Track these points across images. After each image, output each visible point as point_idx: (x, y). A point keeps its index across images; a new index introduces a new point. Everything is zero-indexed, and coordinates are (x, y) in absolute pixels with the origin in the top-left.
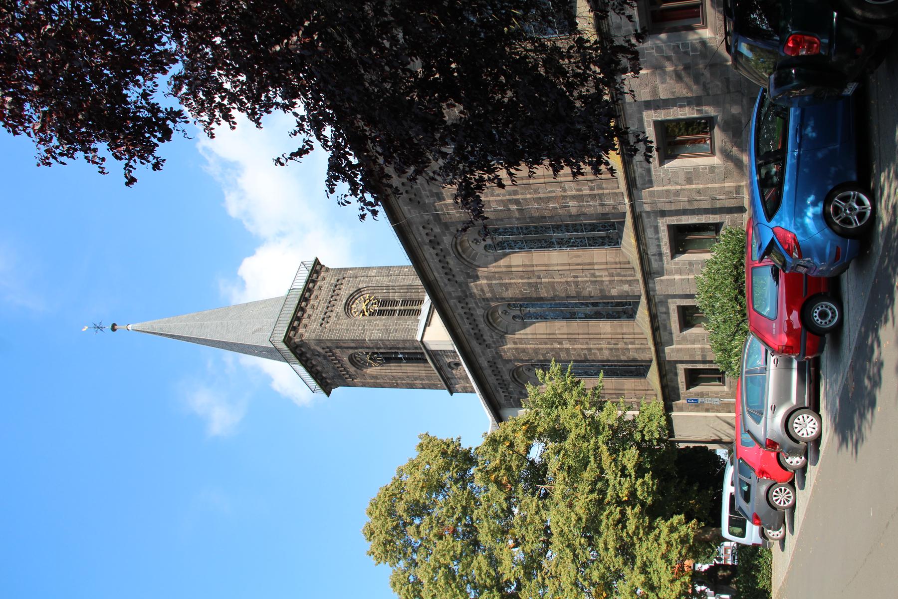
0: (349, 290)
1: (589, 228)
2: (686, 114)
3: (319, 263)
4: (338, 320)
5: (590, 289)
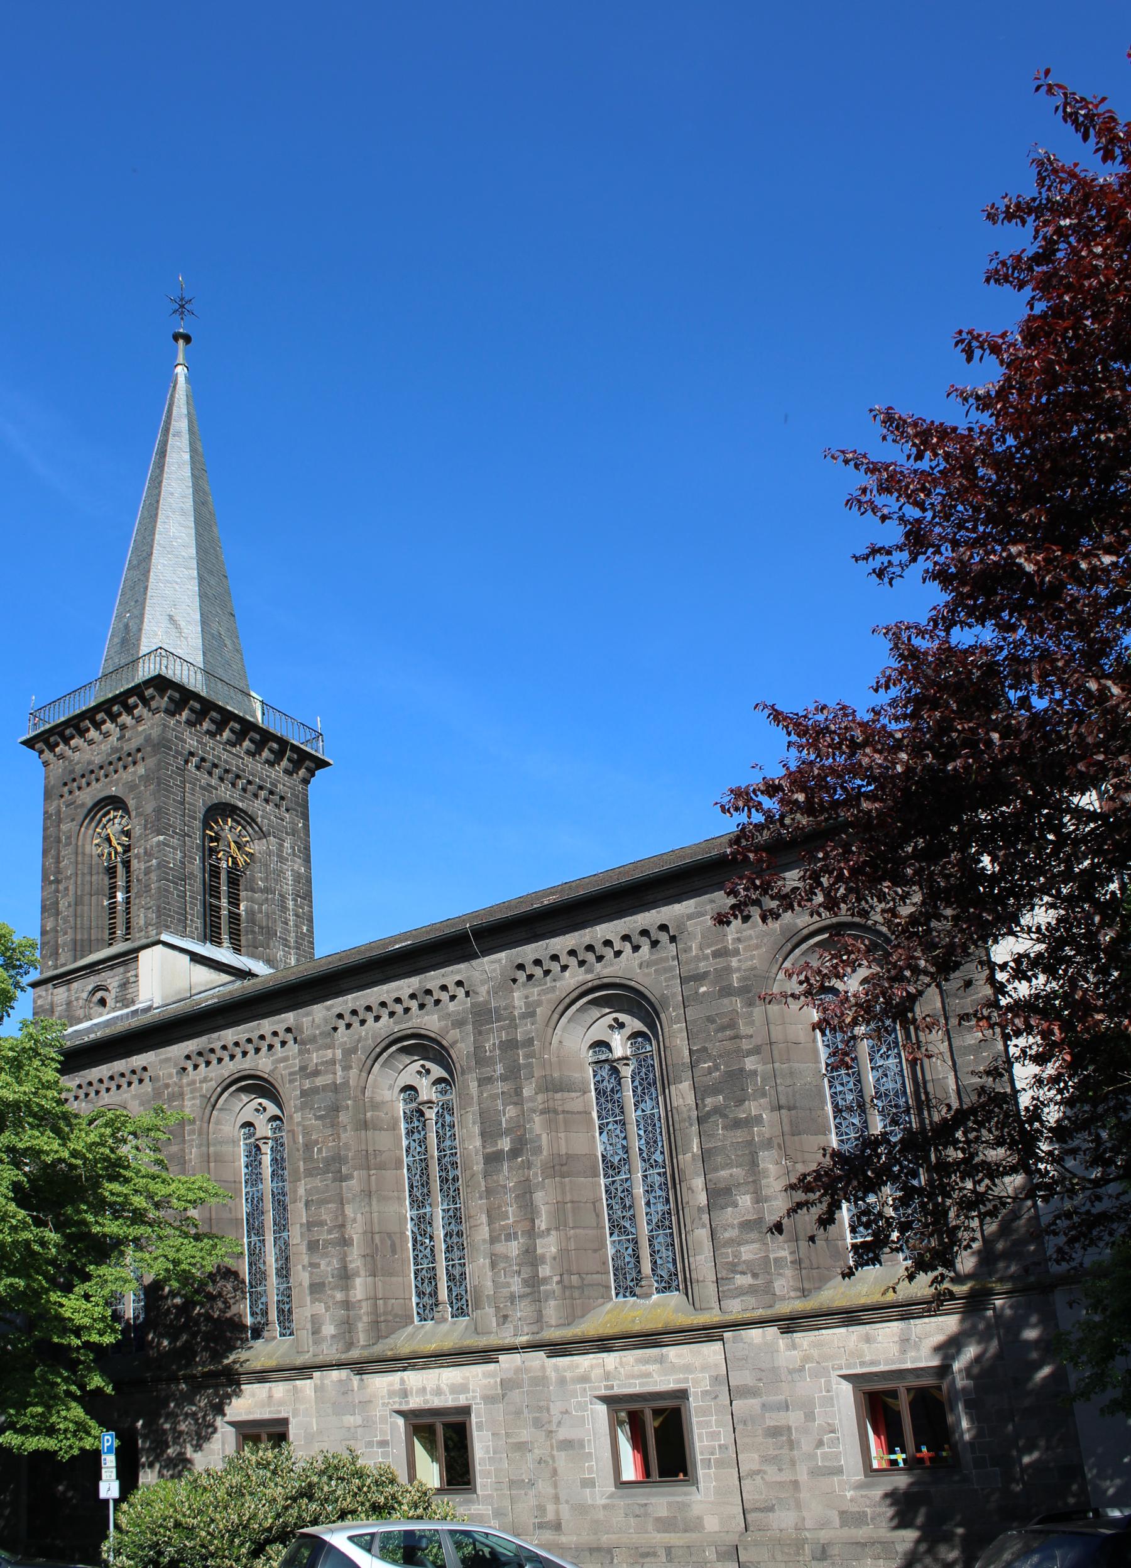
0: (263, 817)
1: (456, 1272)
2: (702, 1441)
3: (318, 767)
4: (202, 788)
5: (322, 1267)
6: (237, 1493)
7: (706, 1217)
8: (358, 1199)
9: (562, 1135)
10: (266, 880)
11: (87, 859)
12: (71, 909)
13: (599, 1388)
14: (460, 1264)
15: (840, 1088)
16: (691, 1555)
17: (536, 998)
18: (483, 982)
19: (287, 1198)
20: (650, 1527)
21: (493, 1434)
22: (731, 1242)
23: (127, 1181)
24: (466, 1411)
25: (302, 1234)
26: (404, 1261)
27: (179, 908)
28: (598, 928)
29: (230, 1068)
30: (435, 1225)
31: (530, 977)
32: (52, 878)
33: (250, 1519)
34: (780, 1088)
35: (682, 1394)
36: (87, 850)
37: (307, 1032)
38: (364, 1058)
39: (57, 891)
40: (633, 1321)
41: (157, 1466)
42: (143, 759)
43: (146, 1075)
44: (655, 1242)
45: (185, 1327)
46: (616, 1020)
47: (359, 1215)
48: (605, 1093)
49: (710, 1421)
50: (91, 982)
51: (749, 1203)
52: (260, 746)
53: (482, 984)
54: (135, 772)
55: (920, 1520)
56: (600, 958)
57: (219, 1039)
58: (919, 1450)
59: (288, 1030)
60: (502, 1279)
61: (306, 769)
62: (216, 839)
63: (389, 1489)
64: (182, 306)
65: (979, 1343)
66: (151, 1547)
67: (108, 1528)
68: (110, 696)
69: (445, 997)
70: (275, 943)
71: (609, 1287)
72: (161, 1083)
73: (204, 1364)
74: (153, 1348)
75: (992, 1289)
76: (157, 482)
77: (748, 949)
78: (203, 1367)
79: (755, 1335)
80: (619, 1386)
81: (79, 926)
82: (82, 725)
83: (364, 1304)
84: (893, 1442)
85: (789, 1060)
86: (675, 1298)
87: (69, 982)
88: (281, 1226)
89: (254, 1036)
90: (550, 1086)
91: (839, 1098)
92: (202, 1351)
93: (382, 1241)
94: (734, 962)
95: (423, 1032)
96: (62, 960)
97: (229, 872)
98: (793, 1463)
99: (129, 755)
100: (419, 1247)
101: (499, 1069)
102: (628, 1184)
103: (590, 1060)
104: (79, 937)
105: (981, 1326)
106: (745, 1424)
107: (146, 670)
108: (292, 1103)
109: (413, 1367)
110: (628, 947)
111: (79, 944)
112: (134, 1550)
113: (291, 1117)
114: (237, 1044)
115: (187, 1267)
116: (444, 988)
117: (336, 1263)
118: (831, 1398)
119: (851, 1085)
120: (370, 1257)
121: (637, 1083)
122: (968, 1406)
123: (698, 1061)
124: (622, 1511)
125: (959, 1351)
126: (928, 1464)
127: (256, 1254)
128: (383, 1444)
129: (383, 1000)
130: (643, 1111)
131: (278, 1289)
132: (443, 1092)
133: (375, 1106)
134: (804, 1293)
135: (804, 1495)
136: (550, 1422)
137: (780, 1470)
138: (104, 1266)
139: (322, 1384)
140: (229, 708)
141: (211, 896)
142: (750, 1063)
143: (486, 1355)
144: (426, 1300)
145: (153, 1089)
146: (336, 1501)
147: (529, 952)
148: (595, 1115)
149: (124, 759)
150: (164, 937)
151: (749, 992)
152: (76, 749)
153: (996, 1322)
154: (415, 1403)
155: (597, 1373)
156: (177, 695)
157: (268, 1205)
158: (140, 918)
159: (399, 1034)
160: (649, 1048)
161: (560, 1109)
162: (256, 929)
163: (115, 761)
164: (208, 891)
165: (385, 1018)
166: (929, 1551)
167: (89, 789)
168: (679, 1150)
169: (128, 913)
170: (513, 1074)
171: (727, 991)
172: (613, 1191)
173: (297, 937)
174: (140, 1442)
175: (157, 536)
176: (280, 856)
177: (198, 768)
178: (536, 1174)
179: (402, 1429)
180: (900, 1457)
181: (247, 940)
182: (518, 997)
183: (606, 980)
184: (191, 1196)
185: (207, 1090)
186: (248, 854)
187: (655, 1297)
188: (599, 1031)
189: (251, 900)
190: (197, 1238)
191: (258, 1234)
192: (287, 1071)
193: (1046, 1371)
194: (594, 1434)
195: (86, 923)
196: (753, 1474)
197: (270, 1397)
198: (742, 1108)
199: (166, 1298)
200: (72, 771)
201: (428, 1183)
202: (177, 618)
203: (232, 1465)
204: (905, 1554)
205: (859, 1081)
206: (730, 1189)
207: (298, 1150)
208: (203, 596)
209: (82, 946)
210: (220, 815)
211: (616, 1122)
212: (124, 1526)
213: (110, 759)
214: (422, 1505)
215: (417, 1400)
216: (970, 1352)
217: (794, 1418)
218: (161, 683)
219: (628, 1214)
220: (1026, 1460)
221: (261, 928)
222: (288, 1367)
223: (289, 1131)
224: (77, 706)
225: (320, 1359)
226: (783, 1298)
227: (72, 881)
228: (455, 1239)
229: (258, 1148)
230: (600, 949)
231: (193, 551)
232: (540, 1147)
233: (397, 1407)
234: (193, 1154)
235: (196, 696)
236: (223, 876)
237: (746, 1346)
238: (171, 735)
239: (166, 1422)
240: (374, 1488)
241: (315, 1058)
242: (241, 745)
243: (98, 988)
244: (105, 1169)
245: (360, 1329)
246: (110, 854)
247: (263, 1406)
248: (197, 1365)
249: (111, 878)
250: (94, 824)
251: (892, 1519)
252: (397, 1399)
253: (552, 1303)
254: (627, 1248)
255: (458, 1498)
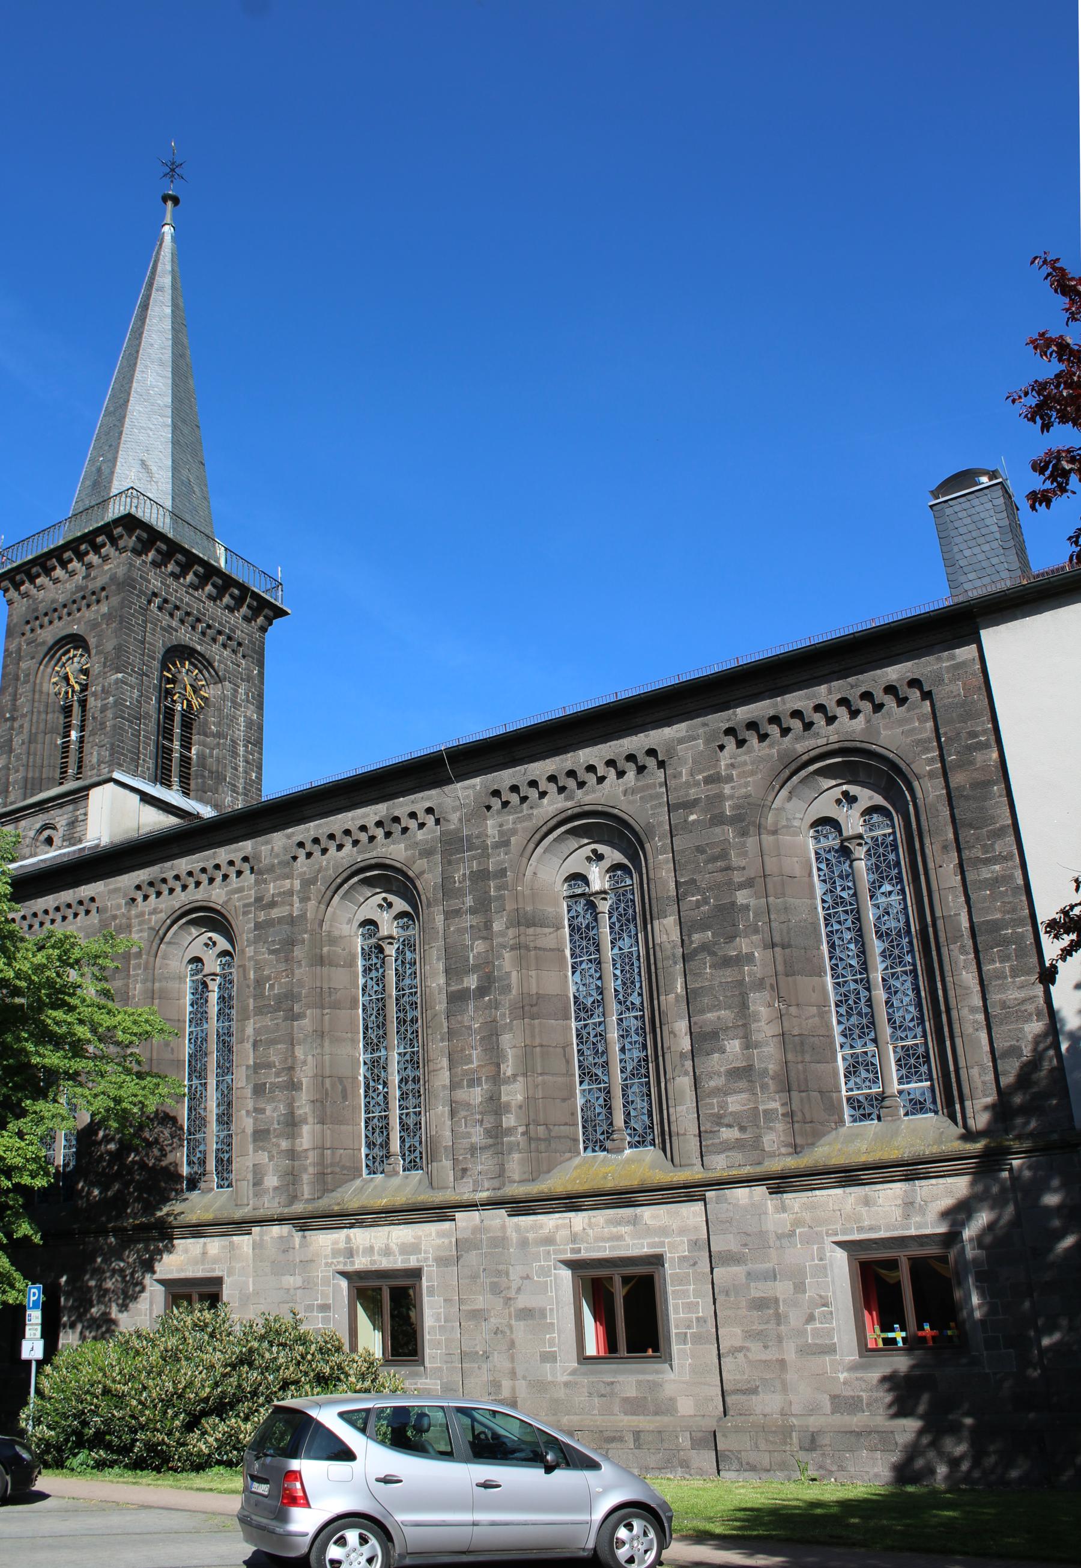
0: (220, 662)
1: (411, 1121)
2: (677, 1312)
3: (276, 617)
4: (162, 628)
5: (268, 1113)
6: (172, 1357)
7: (688, 1064)
8: (309, 1040)
9: (533, 973)
10: (218, 724)
11: (44, 697)
12: (24, 747)
13: (564, 1251)
14: (415, 1113)
15: (836, 927)
16: (662, 1440)
17: (511, 826)
18: (455, 809)
19: (234, 1039)
20: (616, 1409)
21: (445, 1300)
22: (717, 1091)
23: (72, 1009)
24: (416, 1274)
25: (247, 1077)
26: (355, 1109)
27: (133, 747)
28: (581, 752)
29: (182, 899)
30: (390, 1070)
31: (505, 804)
32: (8, 715)
33: (185, 1387)
34: (773, 924)
35: (657, 1260)
36: (45, 688)
37: (265, 861)
38: (323, 889)
39: (12, 728)
40: (605, 1178)
41: (79, 1327)
42: (107, 597)
43: (93, 907)
44: (630, 1092)
45: (118, 1176)
46: (594, 851)
47: (310, 1057)
48: (579, 929)
49: (688, 1290)
50: (39, 821)
51: (738, 1049)
52: (221, 591)
53: (454, 811)
54: (97, 611)
55: (921, 1409)
56: (581, 785)
57: (172, 868)
58: (920, 1328)
59: (245, 859)
60: (463, 1129)
61: (265, 617)
62: (173, 681)
63: (336, 1358)
64: (173, 170)
65: (992, 1208)
66: (75, 1417)
67: (29, 1393)
68: (79, 534)
69: (413, 824)
70: (224, 788)
71: (576, 1140)
72: (108, 914)
73: (135, 1216)
74: (82, 1198)
75: (1009, 1147)
76: (138, 334)
77: (741, 775)
78: (135, 1219)
79: (741, 1195)
80: (586, 1249)
81: (31, 764)
82: (49, 563)
83: (310, 1154)
84: (889, 1318)
85: (784, 895)
86: (650, 1154)
87: (17, 820)
88: (225, 1068)
89: (209, 865)
90: (522, 920)
91: (835, 938)
92: (134, 1202)
93: (333, 1085)
94: (727, 789)
95: (388, 862)
96: (11, 798)
97: (183, 715)
98: (780, 1339)
99: (94, 593)
100: (371, 1093)
101: (469, 901)
102: (602, 1028)
103: (565, 894)
104: (30, 775)
105: (995, 1189)
106: (727, 1294)
107: (116, 510)
108: (245, 936)
109: (360, 1224)
110: (612, 773)
111: (30, 781)
112: (57, 1419)
113: (243, 951)
114: (190, 874)
115: (129, 1106)
116: (413, 815)
117: (282, 1109)
118: (825, 1267)
119: (849, 924)
120: (319, 1103)
121: (614, 919)
122: (981, 1278)
123: (686, 894)
124: (585, 1390)
125: (969, 1217)
126: (931, 1344)
127: (196, 1098)
128: (325, 1308)
129: (347, 827)
130: (620, 949)
131: (218, 1136)
132: (405, 928)
133: (333, 941)
134: (796, 1149)
135: (791, 1376)
136: (509, 1288)
137: (766, 1347)
138: (41, 1101)
139: (262, 1240)
140: (194, 551)
141: (165, 738)
142: (742, 897)
143: (441, 1212)
144: (377, 1152)
145: (100, 921)
146: (278, 1369)
147: (505, 777)
148: (568, 953)
149: (88, 597)
150: (116, 775)
151: (743, 820)
152: (40, 588)
153: (1013, 1184)
154: (361, 1263)
155: (564, 1233)
156: (145, 535)
157: (213, 1046)
158: (92, 756)
159: (362, 864)
160: (629, 882)
161: (532, 945)
162: (206, 773)
163: (79, 600)
164: (161, 733)
165: (348, 847)
166: (933, 1444)
167: (51, 627)
168: (662, 990)
169: (81, 752)
170: (483, 906)
171: (718, 820)
172: (585, 1035)
173: (245, 783)
174: (62, 1299)
175: (134, 384)
176: (234, 702)
177: (160, 608)
178: (504, 1015)
179: (345, 1292)
180: (899, 1335)
181: (197, 783)
182: (491, 826)
183: (587, 808)
184: (136, 1029)
185: (156, 922)
186: (203, 698)
187: (628, 1152)
188: (576, 863)
189: (203, 744)
190: (140, 1076)
191: (199, 1078)
192: (241, 903)
193: (1069, 1241)
194: (557, 1303)
195: (39, 761)
196: (735, 1350)
197: (204, 1253)
198: (732, 945)
199: (100, 1143)
200: (36, 610)
201: (384, 1025)
202: (149, 463)
203: (166, 1327)
204: (905, 1447)
205: (859, 919)
206: (718, 1033)
207: (248, 987)
208: (175, 443)
209: (33, 784)
210: (178, 657)
211: (590, 961)
212: (46, 1391)
213: (74, 597)
214: (370, 1377)
215: (364, 1260)
216: (982, 1218)
217: (782, 1289)
218: (130, 522)
219: (601, 1061)
220: (1046, 1342)
221: (211, 772)
222: (226, 1220)
223: (239, 966)
224: (45, 543)
225: (261, 1213)
226: (772, 1155)
227: (28, 719)
228: (411, 1086)
229: (205, 985)
230: (582, 775)
231: (168, 400)
232: (509, 986)
233: (341, 1268)
234: (137, 989)
235: (163, 537)
236: (177, 718)
237: (731, 1207)
238: (136, 574)
239: (91, 1278)
240: (319, 1356)
241: (272, 888)
242: (203, 590)
243: (46, 827)
244: (49, 996)
245: (305, 1181)
246: (67, 693)
247: (196, 1263)
248: (128, 1216)
249: (66, 717)
250: (53, 663)
251: (890, 1406)
252: (341, 1259)
253: (516, 1156)
254: (598, 1098)
255: (404, 1371)
